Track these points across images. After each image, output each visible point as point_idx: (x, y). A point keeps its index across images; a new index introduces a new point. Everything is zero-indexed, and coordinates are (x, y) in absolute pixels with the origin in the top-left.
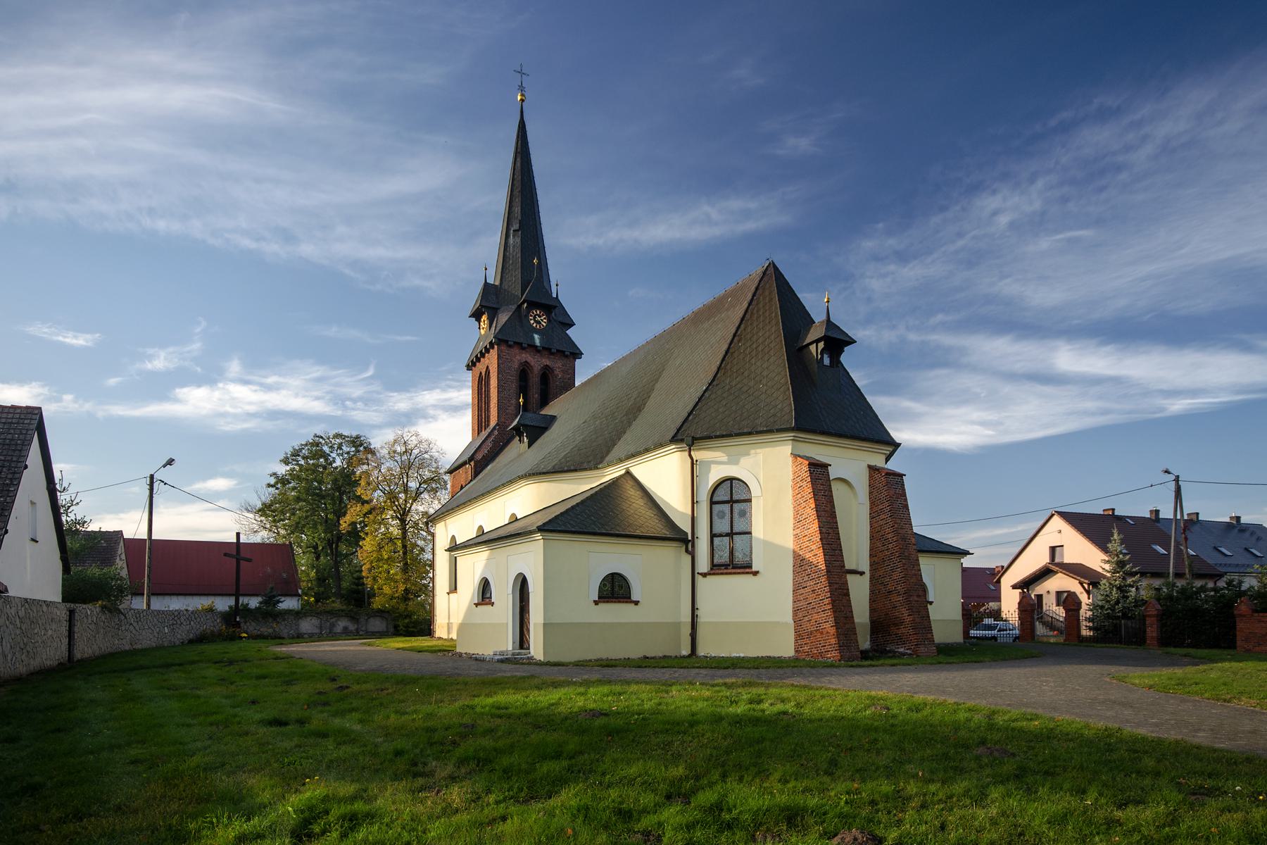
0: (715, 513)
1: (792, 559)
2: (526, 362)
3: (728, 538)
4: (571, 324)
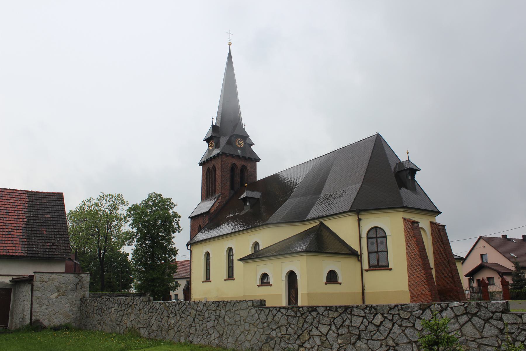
0: (369, 242)
1: (406, 263)
2: (234, 163)
3: (376, 254)
4: (253, 144)
